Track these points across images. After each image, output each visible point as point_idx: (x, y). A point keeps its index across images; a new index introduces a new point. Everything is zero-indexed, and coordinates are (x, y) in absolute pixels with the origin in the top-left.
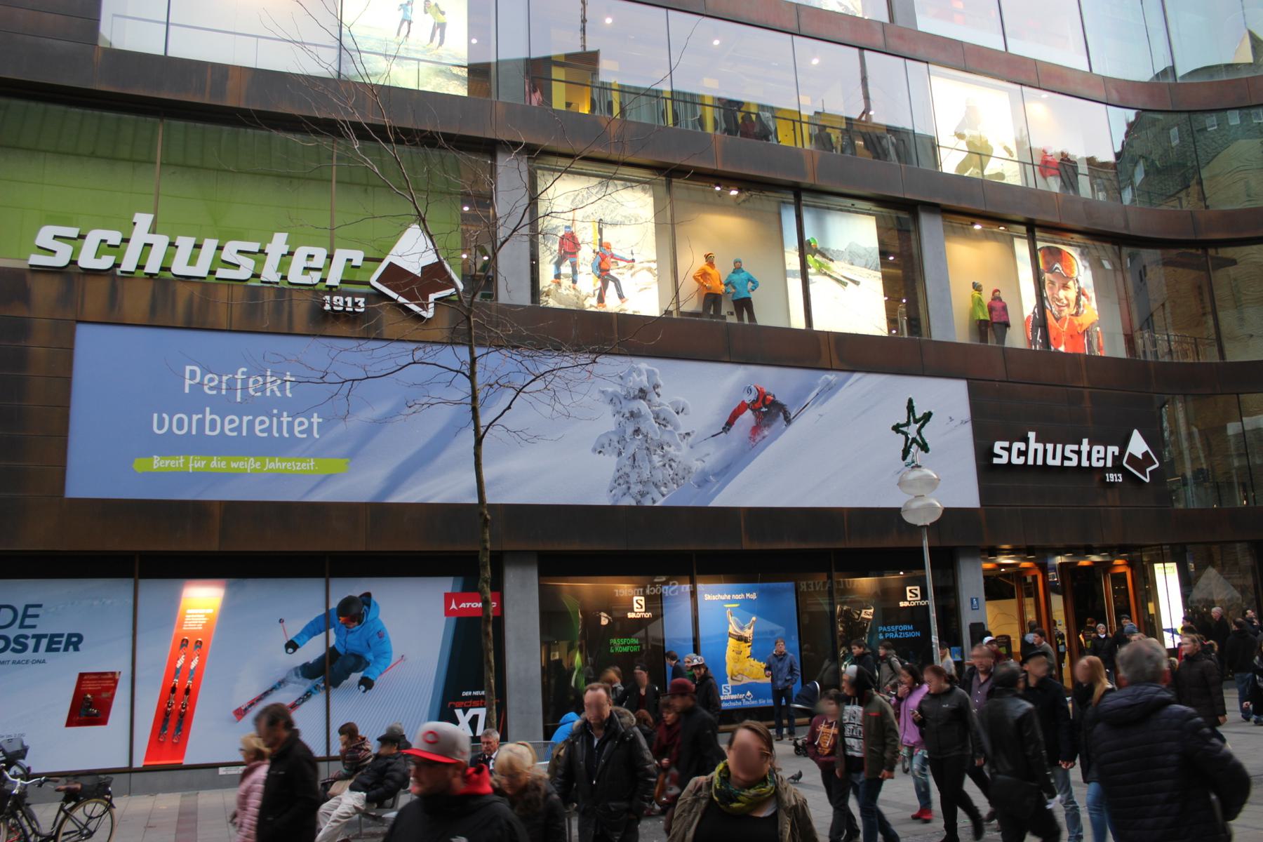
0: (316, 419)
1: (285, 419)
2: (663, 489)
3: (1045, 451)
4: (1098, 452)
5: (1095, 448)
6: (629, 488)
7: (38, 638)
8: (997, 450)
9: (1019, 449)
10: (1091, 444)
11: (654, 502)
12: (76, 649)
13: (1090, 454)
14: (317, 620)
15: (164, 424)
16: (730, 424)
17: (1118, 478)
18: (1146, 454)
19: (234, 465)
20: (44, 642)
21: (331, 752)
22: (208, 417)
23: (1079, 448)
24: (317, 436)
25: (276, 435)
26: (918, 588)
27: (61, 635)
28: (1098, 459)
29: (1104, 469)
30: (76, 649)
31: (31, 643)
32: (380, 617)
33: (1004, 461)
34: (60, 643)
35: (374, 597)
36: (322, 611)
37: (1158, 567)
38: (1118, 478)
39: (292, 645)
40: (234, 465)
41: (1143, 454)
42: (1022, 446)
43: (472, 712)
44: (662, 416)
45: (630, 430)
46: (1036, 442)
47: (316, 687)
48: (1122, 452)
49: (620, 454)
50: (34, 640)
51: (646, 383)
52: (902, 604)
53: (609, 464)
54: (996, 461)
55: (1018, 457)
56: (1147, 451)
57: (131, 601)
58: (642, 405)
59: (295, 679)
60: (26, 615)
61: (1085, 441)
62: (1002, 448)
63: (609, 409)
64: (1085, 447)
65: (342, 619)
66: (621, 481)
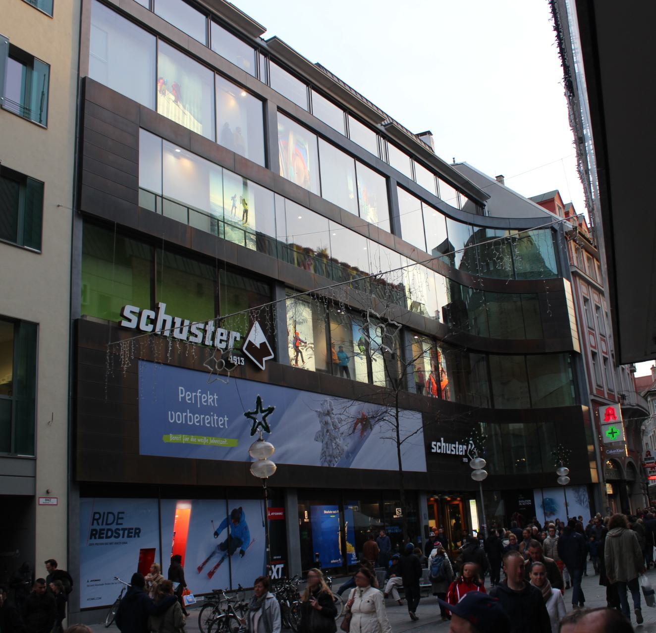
0: (226, 419)
1: (216, 418)
2: (336, 459)
3: (173, 323)
4: (222, 334)
5: (220, 330)
6: (326, 458)
7: (124, 530)
8: (433, 446)
9: (148, 317)
10: (459, 444)
11: (334, 465)
12: (139, 536)
13: (214, 334)
14: (224, 521)
15: (175, 417)
16: (354, 429)
17: (241, 361)
18: (263, 345)
19: (199, 440)
20: (126, 532)
21: (232, 587)
22: (189, 415)
23: (205, 326)
24: (227, 427)
25: (213, 426)
26: (400, 509)
27: (132, 529)
28: (221, 341)
29: (462, 456)
30: (139, 536)
31: (121, 532)
32: (246, 520)
33: (133, 325)
34: (103, 534)
35: (244, 510)
36: (225, 517)
37: (471, 501)
38: (241, 361)
39: (216, 534)
40: (199, 440)
41: (261, 345)
42: (152, 315)
43: (277, 566)
44: (335, 424)
45: (325, 431)
46: (165, 313)
47: (225, 555)
48: (244, 339)
49: (323, 442)
50: (122, 532)
51: (329, 408)
52: (395, 517)
53: (319, 446)
54: (433, 451)
55: (147, 325)
56: (265, 342)
57: (157, 510)
58: (328, 418)
59: (218, 551)
60: (118, 517)
61: (211, 323)
62: (131, 312)
63: (318, 420)
64: (210, 327)
65: (233, 520)
66: (323, 455)
